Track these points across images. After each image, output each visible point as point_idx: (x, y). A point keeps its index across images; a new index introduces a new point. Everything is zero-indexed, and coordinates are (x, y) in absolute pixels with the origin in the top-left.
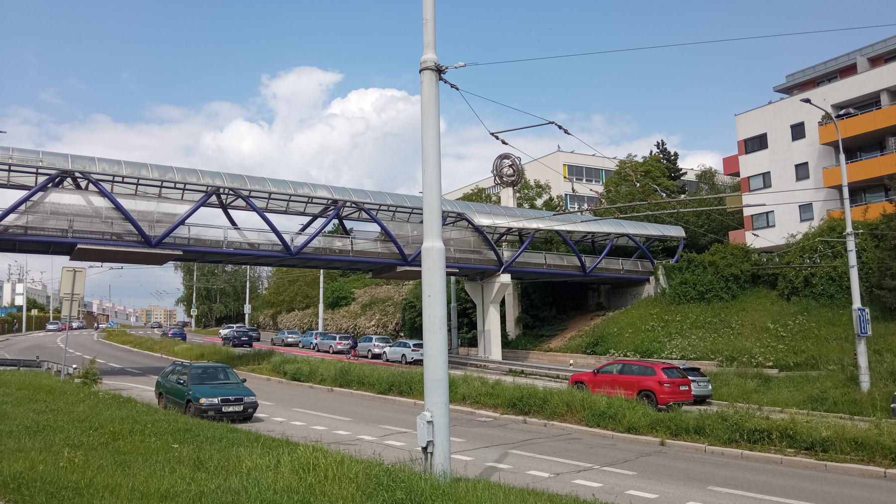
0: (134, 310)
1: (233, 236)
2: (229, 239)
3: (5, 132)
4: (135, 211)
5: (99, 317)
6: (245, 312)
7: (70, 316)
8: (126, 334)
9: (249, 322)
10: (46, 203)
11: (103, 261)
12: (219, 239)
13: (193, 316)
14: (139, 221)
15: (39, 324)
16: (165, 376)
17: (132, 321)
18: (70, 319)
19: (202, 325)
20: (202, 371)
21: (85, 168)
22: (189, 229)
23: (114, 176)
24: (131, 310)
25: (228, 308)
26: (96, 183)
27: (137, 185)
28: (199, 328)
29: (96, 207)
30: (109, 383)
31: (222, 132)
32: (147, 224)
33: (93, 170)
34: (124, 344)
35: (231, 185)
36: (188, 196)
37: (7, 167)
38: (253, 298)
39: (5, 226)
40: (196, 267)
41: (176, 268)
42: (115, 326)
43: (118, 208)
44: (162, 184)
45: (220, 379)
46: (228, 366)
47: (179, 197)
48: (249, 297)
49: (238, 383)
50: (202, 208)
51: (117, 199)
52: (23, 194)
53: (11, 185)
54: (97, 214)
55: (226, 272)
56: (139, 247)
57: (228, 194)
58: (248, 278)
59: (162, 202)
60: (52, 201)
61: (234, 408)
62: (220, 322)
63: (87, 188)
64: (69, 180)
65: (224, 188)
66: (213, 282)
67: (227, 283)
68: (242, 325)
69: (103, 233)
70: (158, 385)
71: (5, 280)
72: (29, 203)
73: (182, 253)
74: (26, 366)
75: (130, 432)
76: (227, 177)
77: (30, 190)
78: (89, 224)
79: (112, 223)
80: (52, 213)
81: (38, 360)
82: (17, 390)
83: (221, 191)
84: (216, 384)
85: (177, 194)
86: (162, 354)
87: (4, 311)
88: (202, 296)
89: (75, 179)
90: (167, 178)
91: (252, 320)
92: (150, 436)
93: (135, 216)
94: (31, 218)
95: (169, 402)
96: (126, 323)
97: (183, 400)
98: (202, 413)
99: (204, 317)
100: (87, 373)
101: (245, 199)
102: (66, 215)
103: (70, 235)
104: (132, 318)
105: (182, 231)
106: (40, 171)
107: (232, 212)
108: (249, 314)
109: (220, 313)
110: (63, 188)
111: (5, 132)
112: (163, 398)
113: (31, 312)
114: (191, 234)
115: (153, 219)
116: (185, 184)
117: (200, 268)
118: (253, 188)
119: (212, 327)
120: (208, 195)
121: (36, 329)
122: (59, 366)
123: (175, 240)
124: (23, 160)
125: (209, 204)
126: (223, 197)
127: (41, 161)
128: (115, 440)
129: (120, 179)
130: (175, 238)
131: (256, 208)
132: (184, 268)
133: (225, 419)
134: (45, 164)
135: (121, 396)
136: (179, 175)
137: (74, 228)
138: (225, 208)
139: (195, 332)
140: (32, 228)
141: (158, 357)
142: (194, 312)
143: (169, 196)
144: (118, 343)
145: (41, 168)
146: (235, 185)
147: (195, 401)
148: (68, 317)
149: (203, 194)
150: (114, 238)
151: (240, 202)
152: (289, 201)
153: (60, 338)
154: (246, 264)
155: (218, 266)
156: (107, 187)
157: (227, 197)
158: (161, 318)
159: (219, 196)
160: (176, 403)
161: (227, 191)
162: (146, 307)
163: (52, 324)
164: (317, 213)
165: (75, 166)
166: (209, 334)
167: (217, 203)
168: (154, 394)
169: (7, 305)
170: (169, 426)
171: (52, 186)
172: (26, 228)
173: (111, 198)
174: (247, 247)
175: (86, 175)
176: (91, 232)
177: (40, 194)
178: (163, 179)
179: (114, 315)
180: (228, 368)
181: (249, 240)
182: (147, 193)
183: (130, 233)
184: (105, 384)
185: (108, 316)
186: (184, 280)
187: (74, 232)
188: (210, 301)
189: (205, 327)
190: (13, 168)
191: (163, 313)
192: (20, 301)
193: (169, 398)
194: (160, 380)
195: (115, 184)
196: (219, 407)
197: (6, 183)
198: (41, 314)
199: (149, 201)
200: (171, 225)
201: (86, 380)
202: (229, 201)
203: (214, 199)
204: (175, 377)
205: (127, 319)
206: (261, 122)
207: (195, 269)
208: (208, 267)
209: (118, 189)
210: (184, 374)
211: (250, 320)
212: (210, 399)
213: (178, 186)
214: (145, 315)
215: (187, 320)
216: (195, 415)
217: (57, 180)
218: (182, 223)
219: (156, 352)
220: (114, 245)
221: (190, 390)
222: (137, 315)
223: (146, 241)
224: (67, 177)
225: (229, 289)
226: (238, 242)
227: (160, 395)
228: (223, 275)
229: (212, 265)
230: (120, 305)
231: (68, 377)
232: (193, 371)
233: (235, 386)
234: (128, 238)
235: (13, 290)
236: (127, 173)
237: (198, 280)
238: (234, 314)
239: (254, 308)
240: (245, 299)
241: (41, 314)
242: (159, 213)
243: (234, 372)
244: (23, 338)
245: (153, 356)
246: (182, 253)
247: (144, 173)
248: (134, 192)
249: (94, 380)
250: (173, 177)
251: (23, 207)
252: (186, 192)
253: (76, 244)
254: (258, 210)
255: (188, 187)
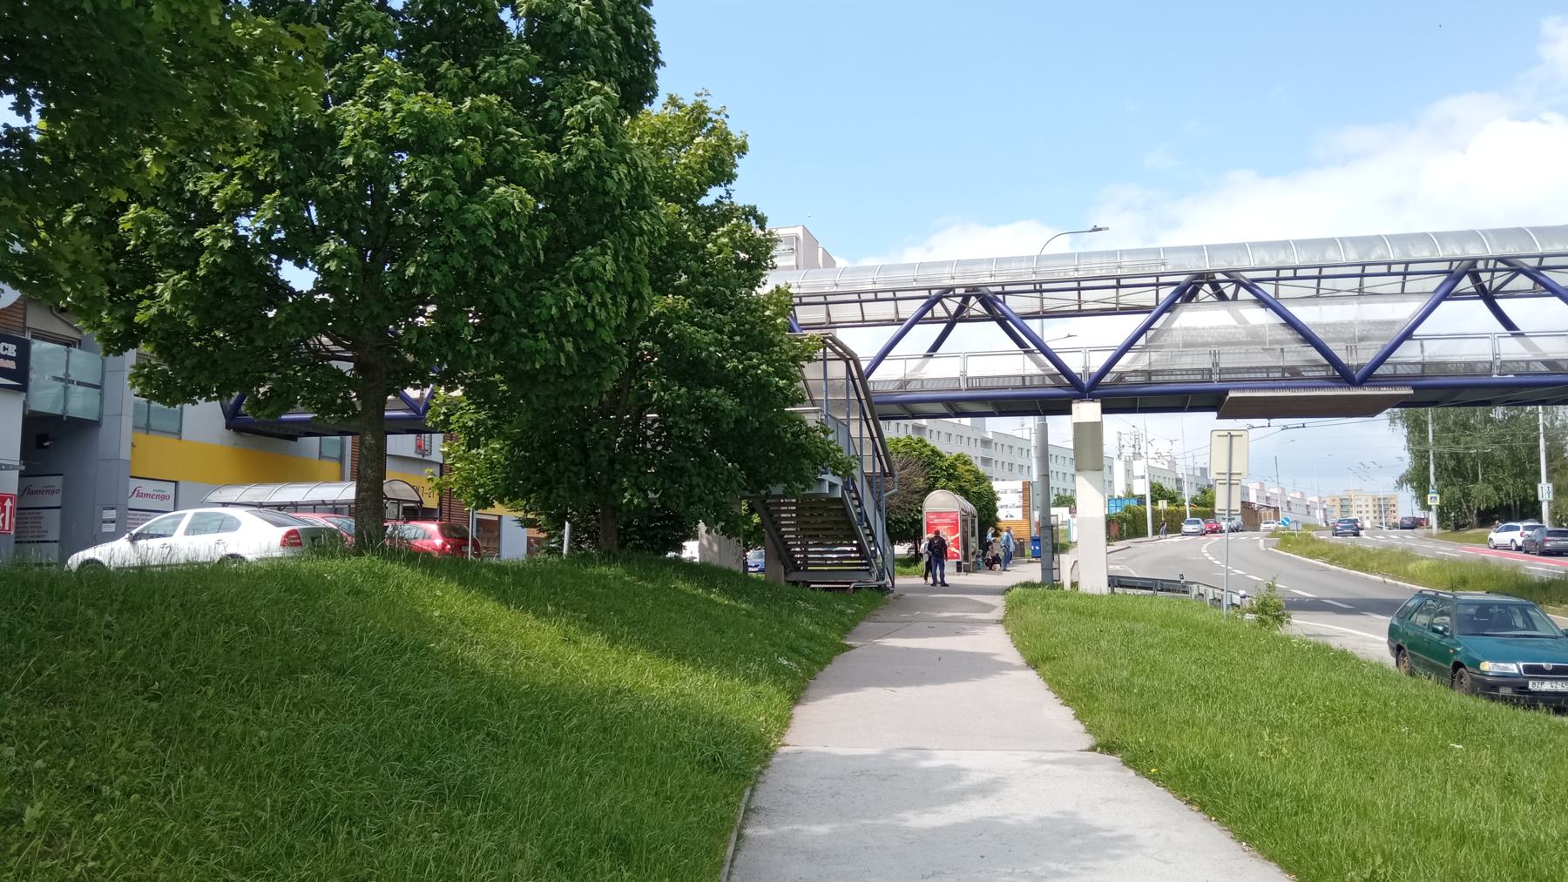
0: (1320, 498)
1: (1512, 349)
2: (1504, 358)
3: (1108, 229)
4: (1319, 325)
5: (1263, 511)
6: (1540, 498)
7: (1230, 511)
8: (1313, 541)
9: (1550, 519)
10: (1176, 329)
11: (1269, 417)
12: (1482, 358)
13: (1433, 507)
14: (1329, 342)
15: (1171, 524)
16: (1405, 614)
17: (1318, 517)
18: (1229, 515)
19: (1452, 525)
20: (1478, 610)
21: (1230, 264)
22: (1422, 345)
23: (1278, 269)
24: (1315, 499)
25: (1502, 490)
26: (1250, 286)
27: (1319, 278)
28: (1445, 528)
29: (1255, 326)
30: (1301, 625)
31: (1464, 153)
32: (1342, 345)
33: (1245, 264)
34: (1313, 558)
35: (1499, 252)
36: (1413, 284)
37: (1113, 282)
38: (1555, 470)
39: (1117, 373)
40: (1430, 416)
41: (1392, 421)
42: (1293, 527)
43: (1291, 323)
44: (1363, 270)
45: (1516, 628)
46: (1531, 603)
47: (1398, 288)
48: (1547, 467)
49: (1556, 637)
50: (1444, 304)
51: (1289, 309)
52: (1141, 319)
53: (1121, 309)
54: (1255, 339)
55: (1491, 420)
56: (1333, 387)
57: (1493, 271)
58: (1541, 430)
59: (1368, 303)
60: (1184, 325)
61: (1554, 685)
62: (1487, 518)
63: (1235, 297)
64: (1207, 287)
65: (1487, 260)
66: (1467, 443)
67: (1498, 442)
68: (1537, 524)
69: (1268, 369)
70: (1393, 632)
71: (1116, 457)
72: (1150, 333)
73: (1412, 392)
74: (1168, 590)
75: (1360, 712)
76: (1491, 237)
77: (1150, 312)
78: (1243, 356)
79: (1282, 350)
80: (1186, 345)
81: (1182, 581)
82: (1162, 626)
83: (1480, 265)
84: (1510, 636)
85: (1393, 284)
86: (1384, 576)
87: (1119, 503)
88: (1446, 469)
89: (1215, 285)
90: (1373, 258)
91: (1556, 513)
92: (1398, 722)
93: (1319, 334)
94: (1154, 356)
95: (1418, 664)
96: (1309, 520)
97: (1448, 664)
98: (1488, 688)
99: (1453, 508)
100: (1264, 604)
101: (1533, 274)
102: (1207, 344)
103: (963, 386)
104: (1317, 512)
105: (1409, 353)
106: (1162, 280)
107: (1502, 303)
108: (1549, 502)
109: (1487, 501)
110: (1198, 302)
111: (1108, 229)
112: (1404, 656)
113: (1157, 504)
114: (1426, 353)
115: (1351, 335)
116: (1407, 264)
117: (1439, 418)
118: (1548, 249)
119: (1471, 528)
120: (1454, 277)
121: (1168, 531)
122: (1217, 591)
123: (1395, 369)
124: (1136, 266)
125: (1456, 294)
126: (1485, 277)
127: (1164, 264)
128: (1337, 723)
129: (1290, 273)
130: (1395, 364)
131: (1557, 289)
132: (1408, 420)
133: (1541, 705)
134: (1169, 267)
135: (1328, 648)
136: (1396, 250)
137: (1221, 366)
138: (1488, 297)
139: (1439, 536)
140: (1157, 372)
141: (1376, 581)
142: (1434, 500)
143: (1378, 290)
144: (1301, 554)
145: (1164, 274)
146: (1509, 250)
147: (1470, 666)
148: (1226, 512)
149: (1443, 278)
150: (1287, 375)
151: (1523, 282)
152: (1362, 276)
153: (1205, 546)
154: (1537, 403)
155: (1475, 411)
156: (1268, 289)
157: (1493, 275)
158: (1367, 512)
159: (1475, 277)
160: (1432, 667)
161: (1491, 264)
162: (1340, 493)
163: (1190, 523)
164: (1562, 285)
165: (1215, 263)
166: (1467, 540)
167: (1473, 290)
168: (1386, 647)
169: (1122, 495)
170: (1431, 707)
171: (1181, 302)
172: (1149, 373)
173: (1278, 307)
174: (1543, 369)
175: (1233, 276)
176: (1249, 370)
177: (1166, 315)
178: (1366, 260)
179: (1286, 509)
180: (1533, 607)
181: (1545, 354)
182: (1339, 291)
183: (1316, 365)
184: (1296, 625)
185: (1276, 509)
186: (1408, 441)
187: (1221, 371)
188: (1465, 478)
189: (1458, 527)
190: (1123, 282)
191: (1370, 503)
192: (1141, 488)
193: (1416, 656)
194: (1395, 623)
195: (1045, 294)
196: (1521, 680)
197: (1114, 306)
198: (1173, 508)
199: (1342, 304)
200: (1386, 343)
201: (1264, 617)
202: (1496, 283)
203: (1466, 284)
204: (1422, 619)
205: (1309, 513)
206: (1547, 116)
207: (1430, 421)
208: (1453, 414)
209: (1285, 290)
210: (1442, 614)
211: (1553, 514)
212: (1502, 665)
213: (1395, 268)
214: (1338, 508)
215: (1419, 514)
216: (1473, 691)
217: (1187, 293)
218: (1408, 335)
219: (1372, 573)
220: (1289, 388)
221: (1458, 644)
222: (1325, 507)
223: (1345, 375)
224: (1202, 284)
225: (1501, 454)
226: (1522, 361)
227: (1398, 650)
228: (1485, 428)
229: (1462, 409)
230: (1294, 491)
231: (1231, 612)
232: (1461, 610)
233: (1549, 642)
234: (1310, 374)
235: (1128, 472)
236: (1301, 260)
237: (1437, 440)
238: (1515, 503)
239: (1558, 490)
240: (1538, 473)
241: (1173, 508)
242: (1363, 323)
243: (1548, 618)
244: (1150, 545)
245: (1367, 579)
246: (1412, 392)
247: (1331, 256)
248: (1314, 292)
249: (1277, 617)
250: (1385, 254)
251: (1142, 341)
252: (1408, 277)
253: (1226, 392)
254: (1561, 291)
255: (1412, 268)
